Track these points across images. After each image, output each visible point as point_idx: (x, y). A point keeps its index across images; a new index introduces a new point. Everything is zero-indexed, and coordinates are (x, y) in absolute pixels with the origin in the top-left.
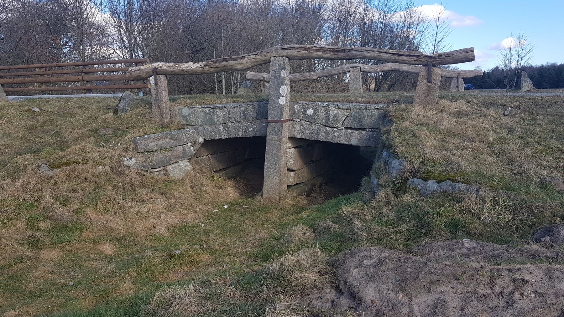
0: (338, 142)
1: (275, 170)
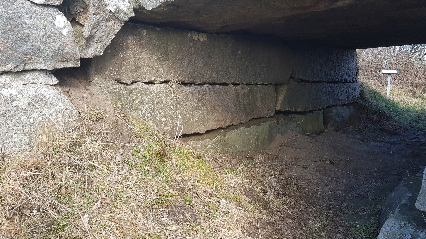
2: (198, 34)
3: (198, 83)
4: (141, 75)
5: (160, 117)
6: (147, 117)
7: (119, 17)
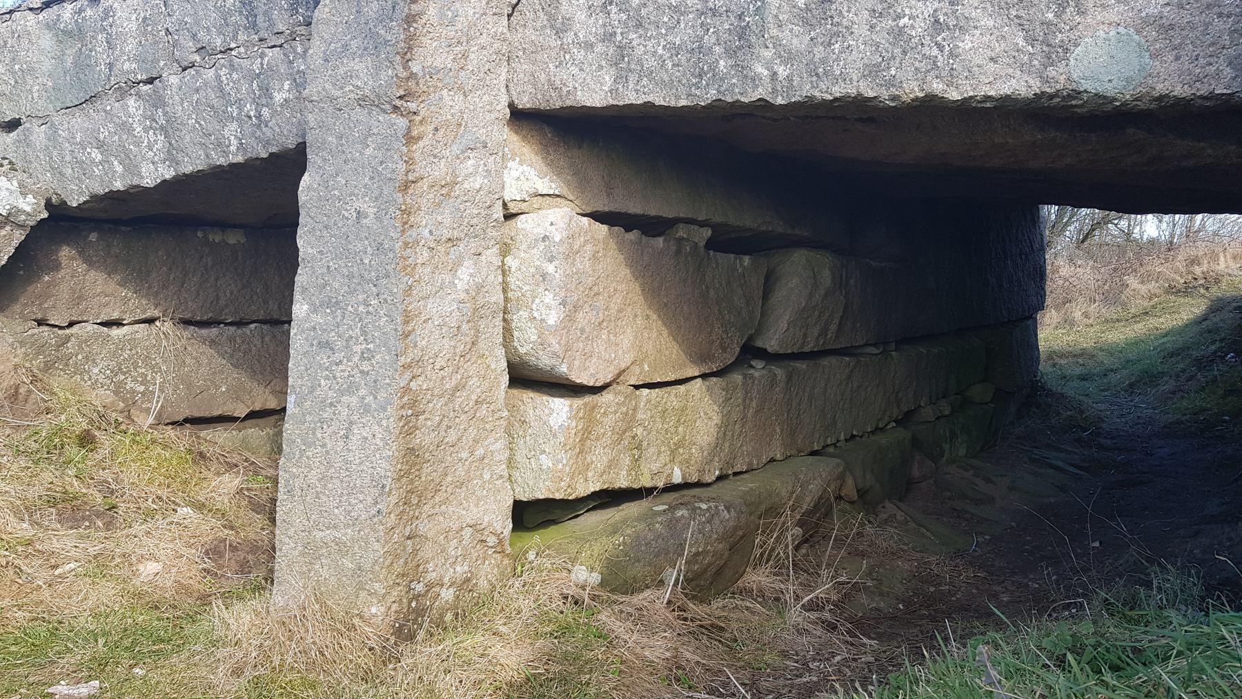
0: (937, 87)
1: (365, 366)
2: (223, 231)
3: (230, 321)
4: (89, 309)
5: (132, 385)
6: (101, 384)
7: (19, 222)
